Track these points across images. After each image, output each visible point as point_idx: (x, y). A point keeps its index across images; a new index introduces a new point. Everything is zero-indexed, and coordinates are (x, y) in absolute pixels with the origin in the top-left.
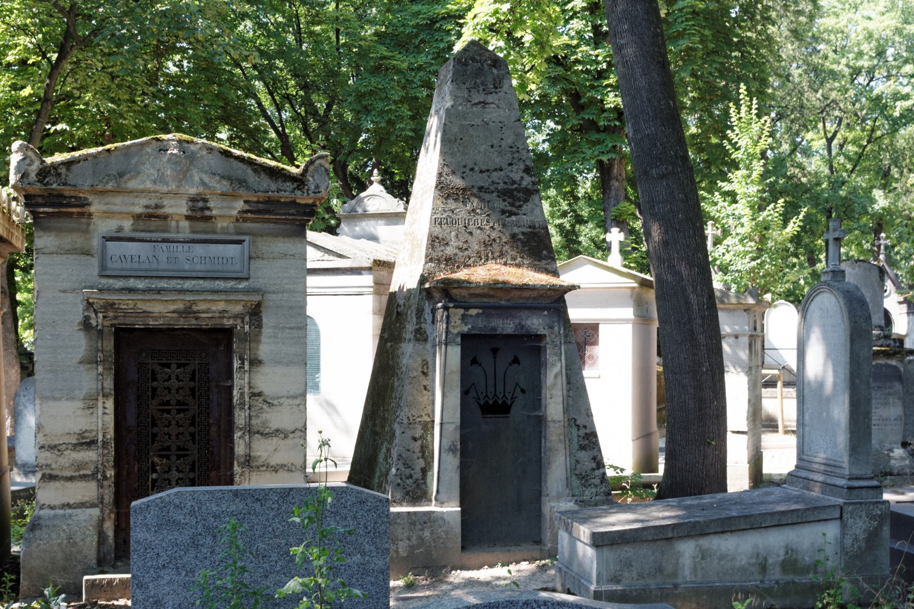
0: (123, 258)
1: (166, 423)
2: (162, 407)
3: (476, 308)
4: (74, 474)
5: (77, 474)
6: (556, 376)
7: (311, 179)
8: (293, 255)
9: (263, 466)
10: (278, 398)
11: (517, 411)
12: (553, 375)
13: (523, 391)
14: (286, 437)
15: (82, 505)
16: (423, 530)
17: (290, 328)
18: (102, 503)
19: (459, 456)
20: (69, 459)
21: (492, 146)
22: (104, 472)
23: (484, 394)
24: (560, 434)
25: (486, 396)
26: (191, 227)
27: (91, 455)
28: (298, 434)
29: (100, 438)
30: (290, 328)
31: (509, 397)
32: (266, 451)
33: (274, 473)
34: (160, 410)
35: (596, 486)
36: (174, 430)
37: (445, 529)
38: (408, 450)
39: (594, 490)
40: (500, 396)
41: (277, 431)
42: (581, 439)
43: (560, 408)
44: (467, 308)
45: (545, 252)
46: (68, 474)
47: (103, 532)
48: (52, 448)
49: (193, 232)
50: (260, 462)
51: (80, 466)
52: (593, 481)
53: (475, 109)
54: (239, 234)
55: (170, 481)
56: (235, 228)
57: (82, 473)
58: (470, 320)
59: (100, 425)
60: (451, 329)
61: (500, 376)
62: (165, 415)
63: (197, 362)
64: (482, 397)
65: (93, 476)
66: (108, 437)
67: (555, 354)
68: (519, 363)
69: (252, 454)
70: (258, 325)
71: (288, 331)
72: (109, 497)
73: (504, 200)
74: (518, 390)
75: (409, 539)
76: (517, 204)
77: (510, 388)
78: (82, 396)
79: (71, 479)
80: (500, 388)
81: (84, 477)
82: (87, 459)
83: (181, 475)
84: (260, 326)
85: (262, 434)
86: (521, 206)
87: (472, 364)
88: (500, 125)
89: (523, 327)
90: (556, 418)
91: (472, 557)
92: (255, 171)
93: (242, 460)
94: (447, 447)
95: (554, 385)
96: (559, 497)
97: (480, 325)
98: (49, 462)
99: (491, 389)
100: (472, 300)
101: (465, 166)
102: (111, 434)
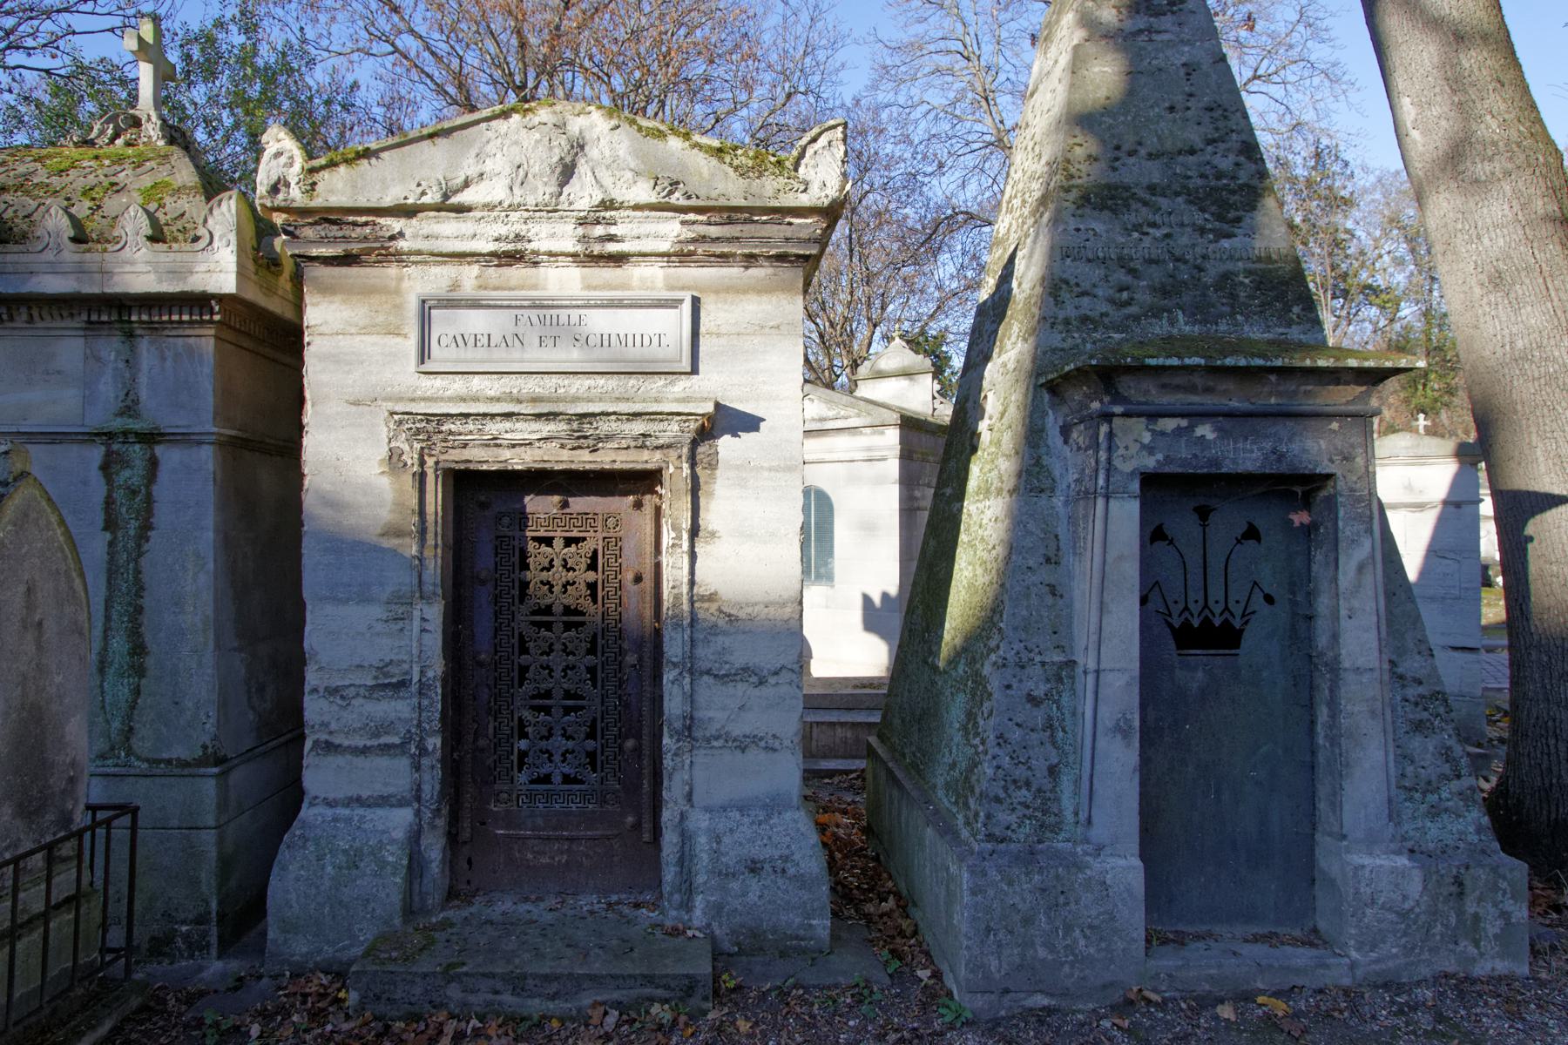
0: (459, 339)
1: (545, 647)
2: (538, 618)
4: (369, 743)
5: (375, 742)
6: (1361, 568)
9: (717, 738)
11: (1261, 642)
12: (1353, 564)
13: (1269, 599)
14: (762, 682)
15: (383, 801)
17: (770, 469)
18: (418, 799)
20: (361, 714)
21: (1172, 109)
22: (422, 739)
23: (1181, 606)
25: (1186, 608)
26: (583, 278)
27: (399, 708)
28: (785, 676)
29: (415, 679)
31: (1237, 610)
32: (724, 709)
33: (738, 752)
34: (533, 623)
36: (557, 660)
40: (1218, 609)
41: (745, 669)
43: (1371, 638)
45: (1296, 309)
46: (360, 742)
47: (419, 852)
48: (331, 694)
49: (588, 287)
50: (712, 730)
51: (384, 727)
54: (672, 288)
55: (551, 755)
56: (666, 278)
57: (383, 740)
59: (415, 651)
60: (1117, 462)
61: (1216, 564)
62: (544, 632)
63: (600, 535)
64: (1176, 610)
65: (402, 748)
66: (430, 674)
68: (1259, 540)
69: (699, 714)
71: (766, 474)
72: (431, 783)
73: (1203, 210)
74: (1258, 598)
76: (1232, 214)
77: (1238, 593)
78: (385, 596)
79: (364, 751)
80: (1216, 592)
81: (386, 749)
82: (393, 716)
83: (570, 744)
85: (716, 676)
86: (1238, 220)
87: (1251, 525)
89: (1281, 457)
90: (1361, 662)
93: (678, 725)
94: (1110, 724)
95: (1358, 587)
96: (1371, 842)
98: (326, 718)
99: (1195, 595)
101: (1118, 148)
102: (437, 667)
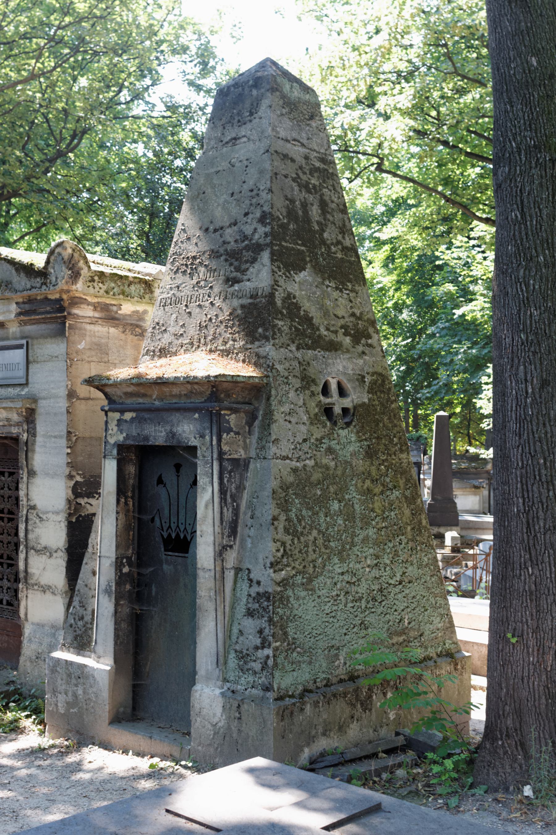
3: (130, 411)
6: (206, 506)
7: (52, 271)
8: (56, 357)
10: (47, 512)
16: (76, 685)
17: (55, 437)
19: (113, 600)
21: (232, 194)
24: (210, 589)
30: (55, 437)
35: (255, 673)
37: (94, 690)
38: (86, 586)
39: (251, 679)
41: (45, 548)
42: (251, 600)
44: (122, 412)
45: (260, 330)
52: (253, 664)
53: (225, 149)
58: (125, 426)
67: (206, 474)
70: (32, 432)
75: (66, 694)
80: (182, 520)
84: (34, 435)
88: (245, 163)
91: (121, 735)
92: (17, 270)
95: (205, 517)
97: (134, 433)
100: (129, 401)
